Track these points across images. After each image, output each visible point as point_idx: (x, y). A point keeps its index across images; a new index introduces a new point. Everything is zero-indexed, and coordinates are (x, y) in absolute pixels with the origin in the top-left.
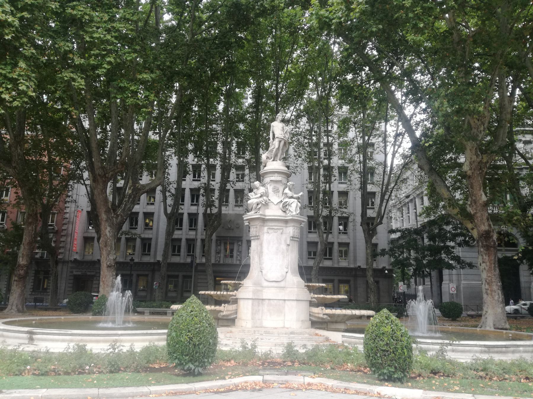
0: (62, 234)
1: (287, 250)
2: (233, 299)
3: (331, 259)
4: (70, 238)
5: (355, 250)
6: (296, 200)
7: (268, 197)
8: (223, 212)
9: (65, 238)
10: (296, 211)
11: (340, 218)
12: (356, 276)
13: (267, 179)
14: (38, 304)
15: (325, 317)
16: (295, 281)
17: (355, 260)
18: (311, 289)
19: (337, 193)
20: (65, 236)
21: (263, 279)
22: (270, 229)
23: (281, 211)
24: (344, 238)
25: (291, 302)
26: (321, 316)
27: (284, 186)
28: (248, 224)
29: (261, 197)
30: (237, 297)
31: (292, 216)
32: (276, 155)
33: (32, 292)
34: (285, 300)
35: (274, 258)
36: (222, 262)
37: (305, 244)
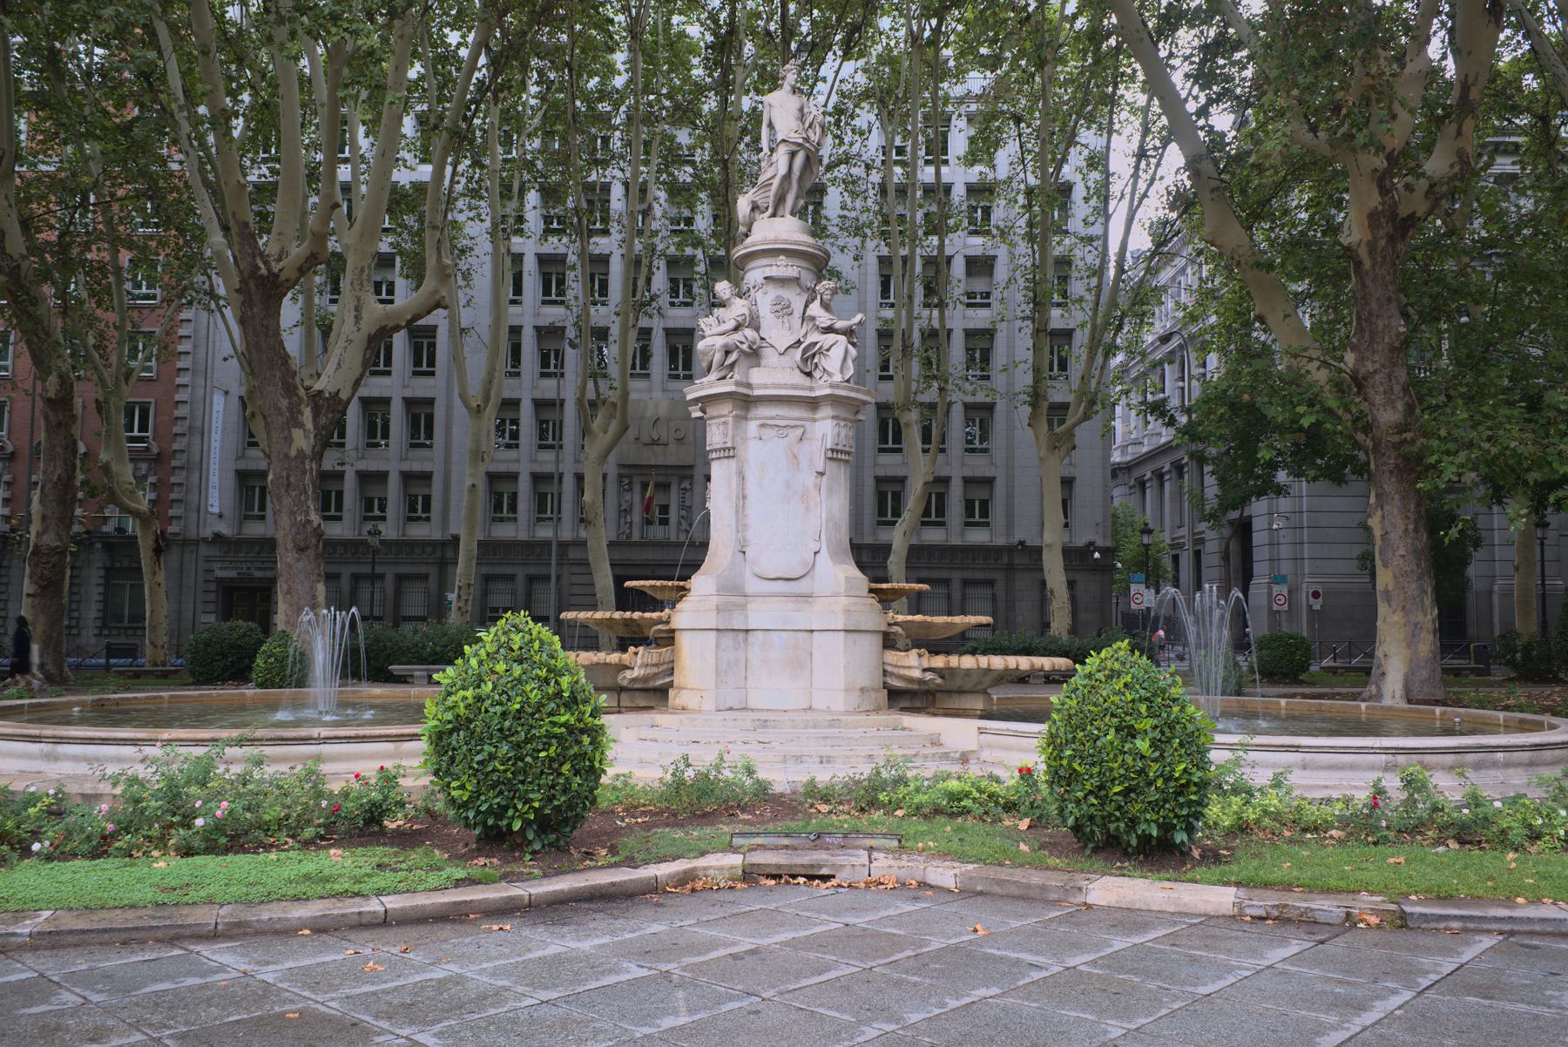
0: (174, 463)
2: (660, 631)
4: (197, 474)
5: (1010, 497)
6: (842, 338)
7: (757, 329)
8: (633, 396)
9: (184, 473)
11: (968, 407)
12: (1010, 569)
13: (754, 275)
14: (112, 661)
15: (929, 676)
16: (839, 578)
17: (1010, 526)
19: (962, 335)
20: (182, 468)
22: (763, 426)
24: (978, 466)
26: (917, 674)
27: (805, 297)
28: (699, 414)
29: (736, 329)
30: (673, 625)
31: (832, 386)
32: (780, 199)
33: (101, 628)
35: (776, 508)
36: (636, 537)
37: (869, 484)
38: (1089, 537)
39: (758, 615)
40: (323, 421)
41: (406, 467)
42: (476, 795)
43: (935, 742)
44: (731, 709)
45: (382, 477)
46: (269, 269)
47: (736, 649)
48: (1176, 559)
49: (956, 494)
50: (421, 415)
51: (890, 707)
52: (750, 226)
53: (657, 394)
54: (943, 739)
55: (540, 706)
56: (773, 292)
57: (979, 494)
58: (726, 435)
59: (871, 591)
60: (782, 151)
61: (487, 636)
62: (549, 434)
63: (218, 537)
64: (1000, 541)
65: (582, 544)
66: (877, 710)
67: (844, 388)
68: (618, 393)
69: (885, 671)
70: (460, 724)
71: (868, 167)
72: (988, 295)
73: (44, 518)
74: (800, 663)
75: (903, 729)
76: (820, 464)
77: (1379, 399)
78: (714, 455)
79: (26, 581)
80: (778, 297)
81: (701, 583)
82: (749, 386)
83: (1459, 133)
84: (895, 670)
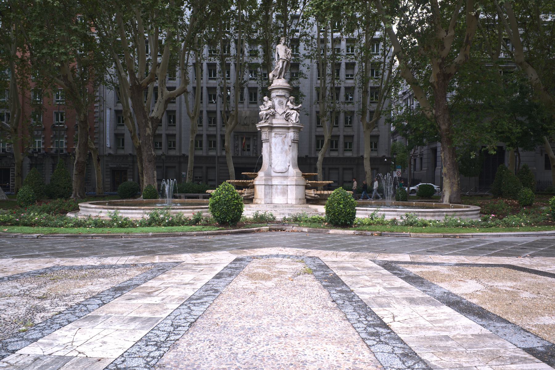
0: (95, 131)
5: (359, 141)
7: (274, 109)
8: (239, 109)
10: (295, 120)
13: (274, 94)
15: (316, 196)
16: (294, 172)
17: (358, 151)
18: (306, 177)
24: (349, 131)
26: (313, 195)
32: (280, 74)
35: (279, 154)
36: (240, 155)
37: (314, 137)
38: (384, 154)
39: (275, 182)
40: (154, 125)
41: (167, 132)
42: (220, 215)
46: (139, 83)
48: (415, 160)
52: (272, 81)
53: (246, 109)
55: (231, 199)
59: (303, 175)
60: (281, 61)
61: (221, 186)
62: (212, 121)
63: (110, 154)
64: (355, 156)
65: (225, 157)
68: (235, 112)
69: (306, 195)
70: (217, 202)
71: (312, 38)
73: (80, 153)
74: (285, 193)
76: (290, 144)
77: (441, 122)
79: (74, 171)
81: (261, 174)
82: (272, 124)
83: (465, 50)
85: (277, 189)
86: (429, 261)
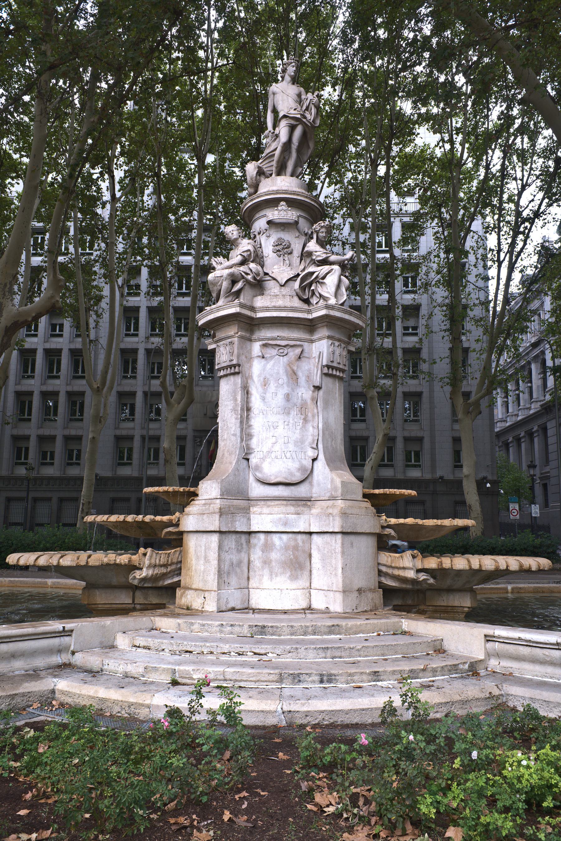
1: (315, 401)
2: (170, 533)
3: (392, 466)
5: (433, 449)
13: (260, 224)
15: (422, 577)
16: (330, 479)
18: (380, 505)
21: (251, 479)
22: (265, 345)
23: (296, 299)
24: (413, 430)
25: (327, 537)
26: (411, 574)
29: (243, 262)
30: (182, 528)
34: (311, 533)
35: (276, 419)
39: (262, 519)
41: (67, 432)
43: (439, 649)
44: (233, 609)
45: (52, 438)
47: (239, 551)
49: (400, 445)
50: (76, 400)
51: (385, 605)
54: (447, 645)
56: (275, 236)
57: (414, 447)
58: (232, 354)
59: (365, 496)
64: (428, 476)
66: (373, 611)
67: (339, 310)
69: (380, 573)
72: (415, 328)
74: (298, 564)
75: (404, 633)
76: (317, 380)
78: (222, 373)
80: (280, 239)
81: (209, 489)
82: (252, 309)
84: (390, 571)
85: (267, 548)
86: (550, 670)
